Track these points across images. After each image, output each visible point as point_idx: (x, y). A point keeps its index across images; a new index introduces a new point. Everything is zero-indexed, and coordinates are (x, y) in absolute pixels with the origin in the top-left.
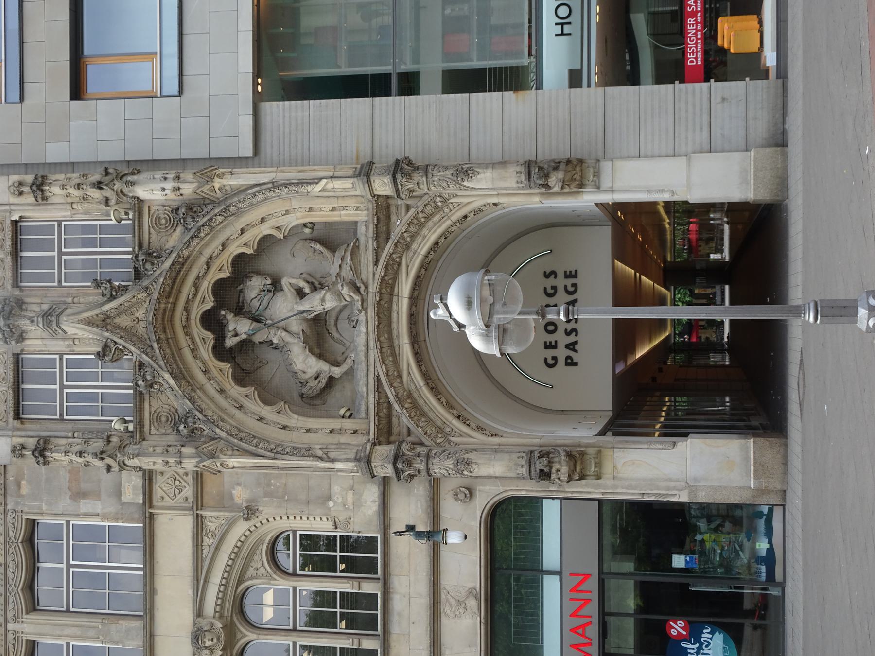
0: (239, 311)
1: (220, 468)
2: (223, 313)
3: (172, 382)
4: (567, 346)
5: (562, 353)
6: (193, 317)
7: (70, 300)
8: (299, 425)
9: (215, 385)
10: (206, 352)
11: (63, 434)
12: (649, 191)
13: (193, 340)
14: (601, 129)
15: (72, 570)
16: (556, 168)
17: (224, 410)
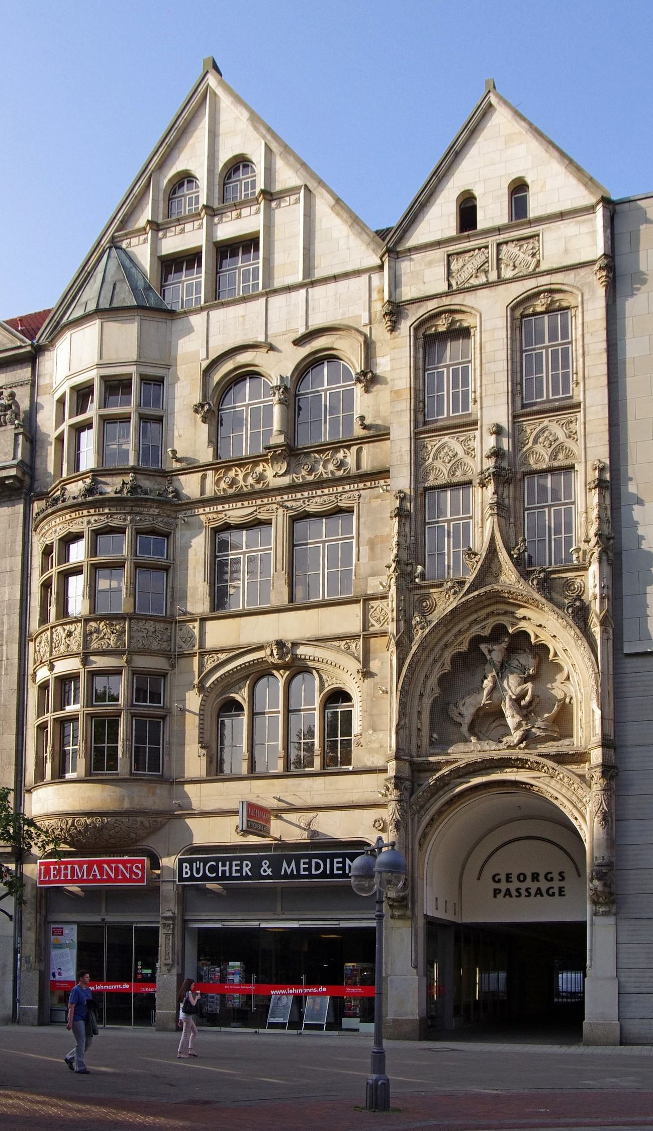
0: (512, 650)
1: (390, 650)
2: (506, 640)
3: (450, 608)
4: (508, 890)
5: (503, 886)
6: (501, 618)
7: (512, 520)
8: (424, 705)
9: (451, 640)
10: (475, 631)
11: (413, 527)
12: (591, 950)
13: (483, 620)
14: (638, 916)
15: (321, 545)
16: (605, 885)
17: (433, 649)
